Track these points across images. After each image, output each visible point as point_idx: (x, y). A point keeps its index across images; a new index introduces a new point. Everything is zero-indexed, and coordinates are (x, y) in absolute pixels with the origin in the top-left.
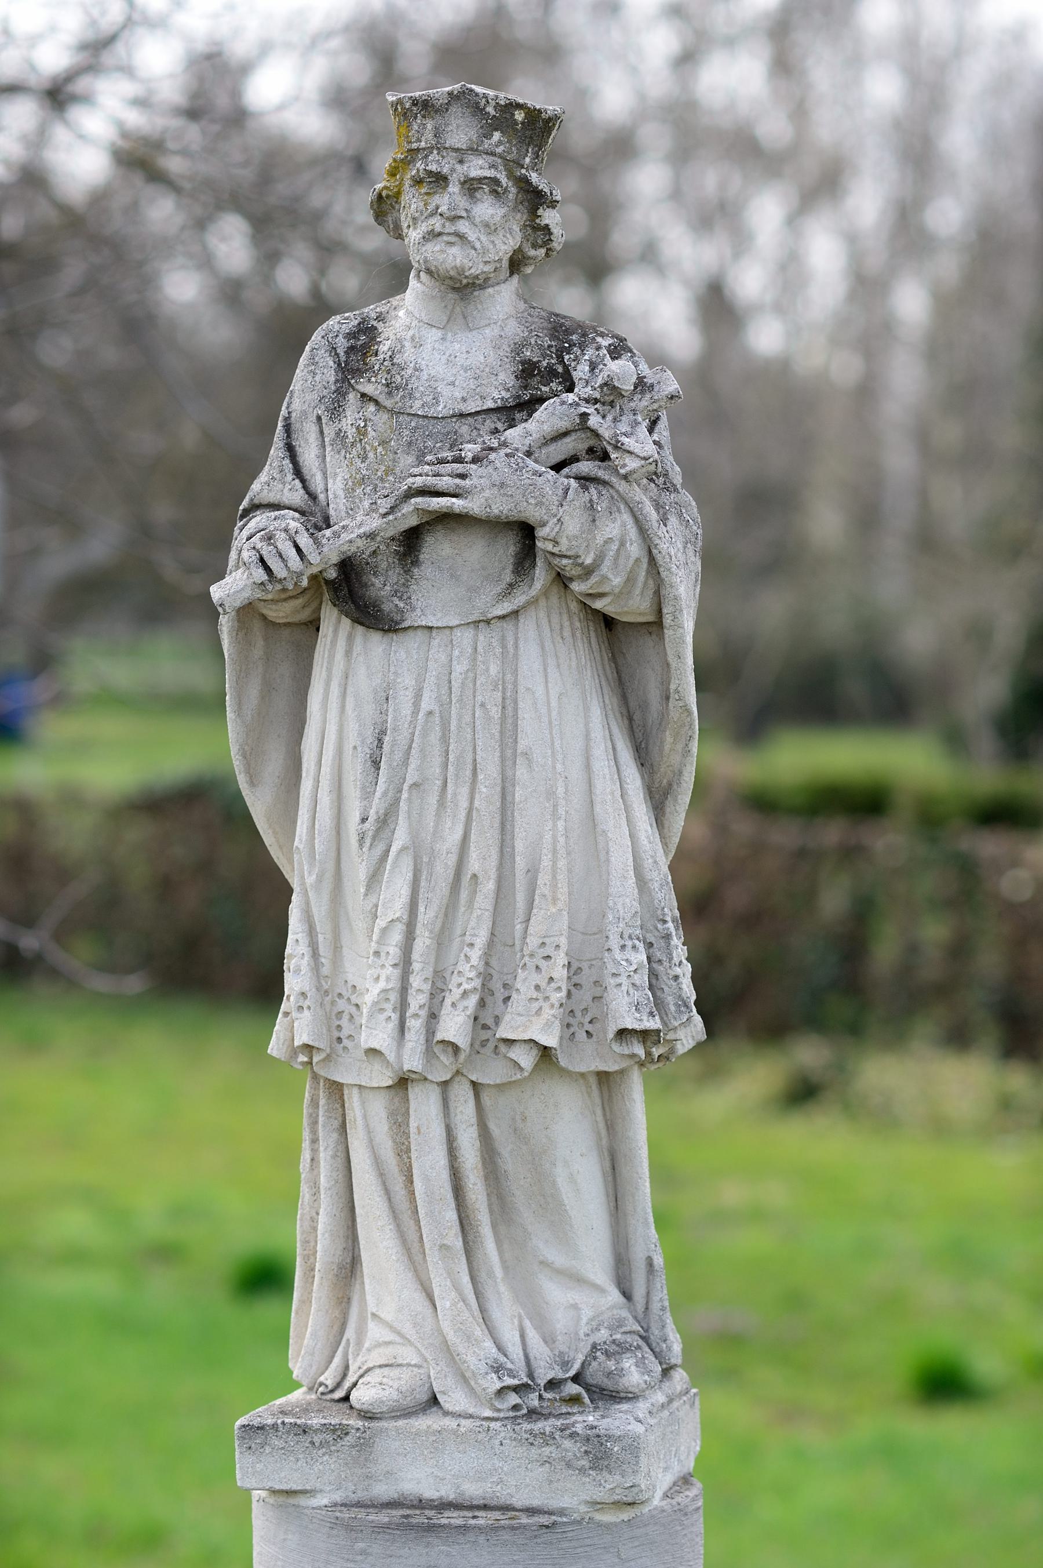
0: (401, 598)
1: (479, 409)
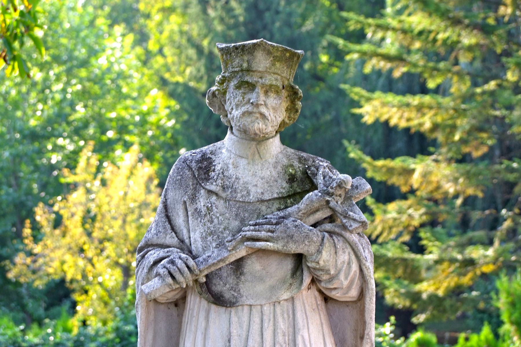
0: (235, 291)
1: (270, 198)
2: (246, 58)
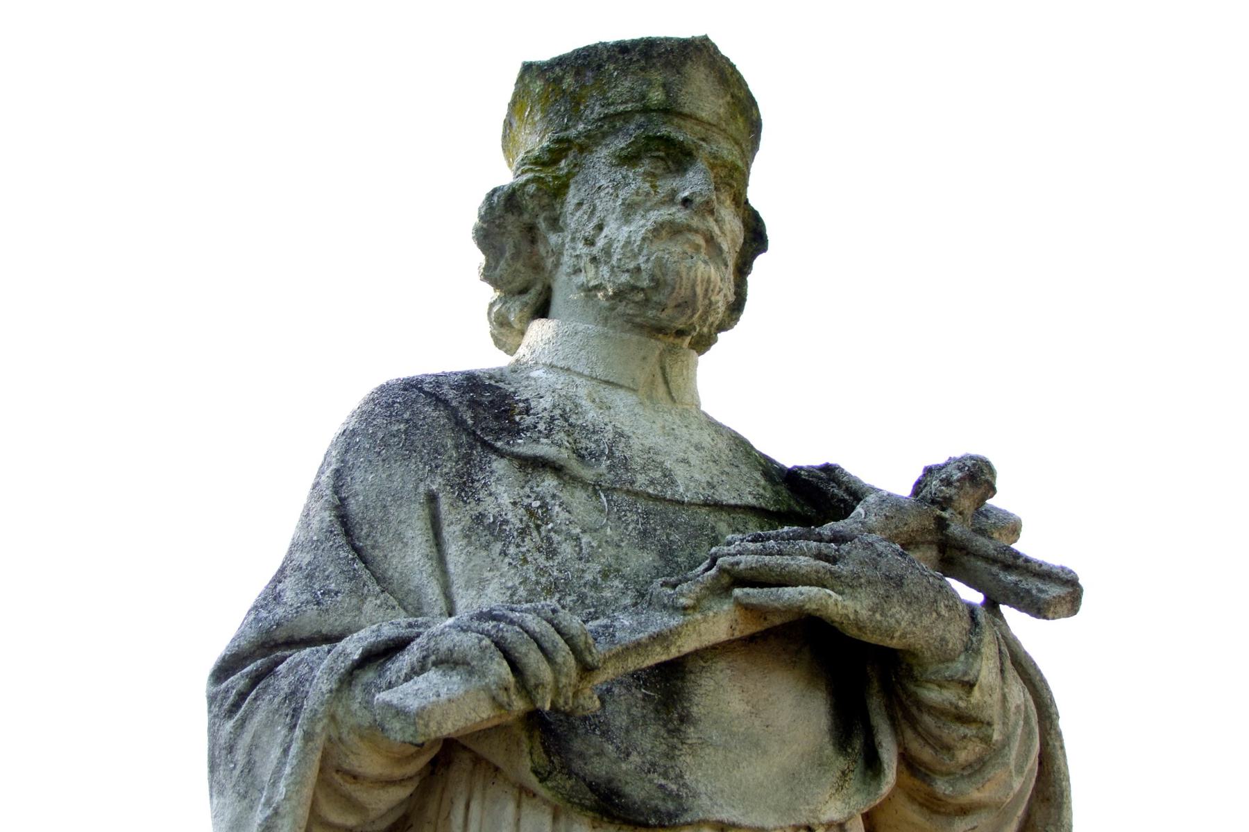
0: (665, 775)
2: (657, 76)
